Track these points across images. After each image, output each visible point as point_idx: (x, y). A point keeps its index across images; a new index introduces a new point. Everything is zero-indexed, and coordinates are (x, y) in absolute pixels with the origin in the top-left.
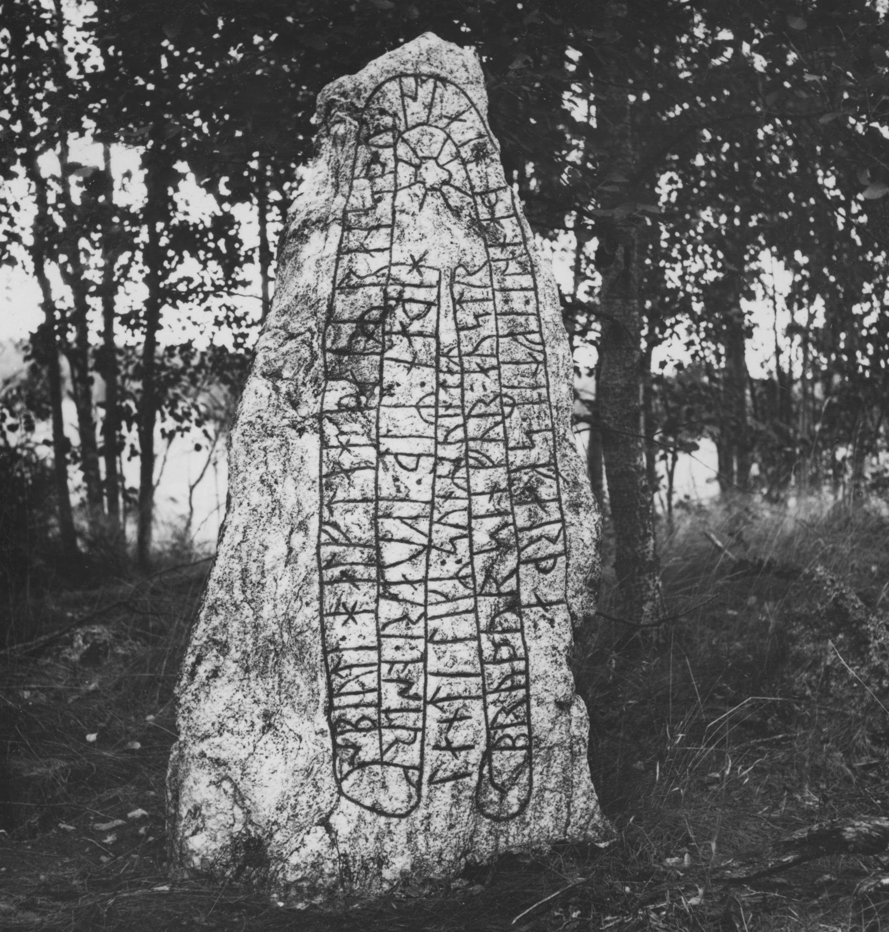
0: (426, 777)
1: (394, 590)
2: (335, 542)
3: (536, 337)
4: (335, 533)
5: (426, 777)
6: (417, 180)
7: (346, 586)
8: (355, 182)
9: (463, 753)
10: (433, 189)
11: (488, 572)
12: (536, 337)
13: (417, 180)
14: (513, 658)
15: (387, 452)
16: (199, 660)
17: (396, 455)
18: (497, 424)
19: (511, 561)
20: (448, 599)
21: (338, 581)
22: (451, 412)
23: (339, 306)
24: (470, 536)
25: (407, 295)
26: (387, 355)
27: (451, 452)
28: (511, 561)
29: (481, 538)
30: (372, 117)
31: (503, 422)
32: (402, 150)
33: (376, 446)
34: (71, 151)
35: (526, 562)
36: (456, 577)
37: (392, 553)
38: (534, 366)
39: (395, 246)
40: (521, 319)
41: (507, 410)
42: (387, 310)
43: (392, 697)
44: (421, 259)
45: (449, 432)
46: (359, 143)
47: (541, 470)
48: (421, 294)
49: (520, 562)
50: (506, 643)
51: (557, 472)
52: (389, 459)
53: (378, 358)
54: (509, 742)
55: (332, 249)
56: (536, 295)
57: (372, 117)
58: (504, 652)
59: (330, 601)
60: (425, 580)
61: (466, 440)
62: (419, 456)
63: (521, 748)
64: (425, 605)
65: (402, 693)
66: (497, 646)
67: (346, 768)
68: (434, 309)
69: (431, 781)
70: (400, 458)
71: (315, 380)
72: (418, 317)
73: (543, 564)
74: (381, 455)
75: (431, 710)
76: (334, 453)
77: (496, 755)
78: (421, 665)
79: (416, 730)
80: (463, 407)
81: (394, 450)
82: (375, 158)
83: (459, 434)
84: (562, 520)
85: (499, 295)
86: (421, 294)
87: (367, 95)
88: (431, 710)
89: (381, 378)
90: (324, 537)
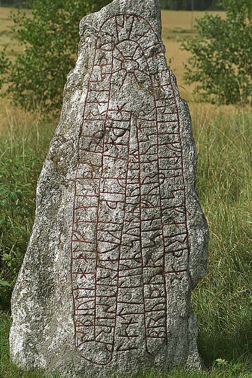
0: (115, 348)
1: (103, 264)
2: (78, 240)
3: (177, 145)
4: (79, 237)
5: (115, 348)
6: (122, 68)
7: (82, 261)
8: (95, 67)
9: (134, 338)
10: (129, 72)
11: (149, 256)
12: (177, 145)
13: (122, 68)
14: (159, 296)
15: (103, 200)
16: (21, 289)
17: (107, 201)
18: (156, 187)
19: (160, 251)
20: (128, 268)
21: (79, 258)
22: (133, 181)
23: (84, 128)
24: (140, 240)
25: (114, 125)
26: (104, 154)
27: (133, 200)
28: (160, 251)
29: (145, 241)
30: (103, 36)
31: (159, 186)
32: (115, 53)
33: (98, 197)
34: (190, 57)
35: (168, 252)
36: (133, 258)
37: (103, 247)
38: (176, 159)
39: (110, 101)
40: (171, 136)
41: (161, 180)
42: (104, 132)
43: (100, 313)
44: (122, 108)
45: (132, 190)
46: (96, 48)
47: (177, 209)
48: (122, 125)
49: (165, 253)
50: (156, 289)
51: (185, 210)
52: (104, 203)
53: (101, 154)
54: (155, 334)
55: (83, 100)
56: (179, 123)
57: (103, 36)
58: (155, 293)
59: (75, 269)
60: (118, 260)
61: (139, 195)
62: (117, 202)
63: (162, 337)
64: (118, 271)
65: (106, 311)
66: (151, 291)
67: (79, 342)
68: (127, 132)
69: (118, 350)
70: (109, 203)
71: (73, 163)
72: (120, 136)
73: (176, 253)
74: (99, 201)
75: (118, 318)
76: (80, 199)
77: (149, 339)
78: (115, 298)
79: (111, 327)
80: (139, 179)
81: (106, 198)
82: (103, 57)
83: (136, 192)
84: (187, 233)
85: (159, 124)
86: (122, 125)
87: (100, 25)
88: (118, 318)
89: (102, 164)
90: (74, 238)
